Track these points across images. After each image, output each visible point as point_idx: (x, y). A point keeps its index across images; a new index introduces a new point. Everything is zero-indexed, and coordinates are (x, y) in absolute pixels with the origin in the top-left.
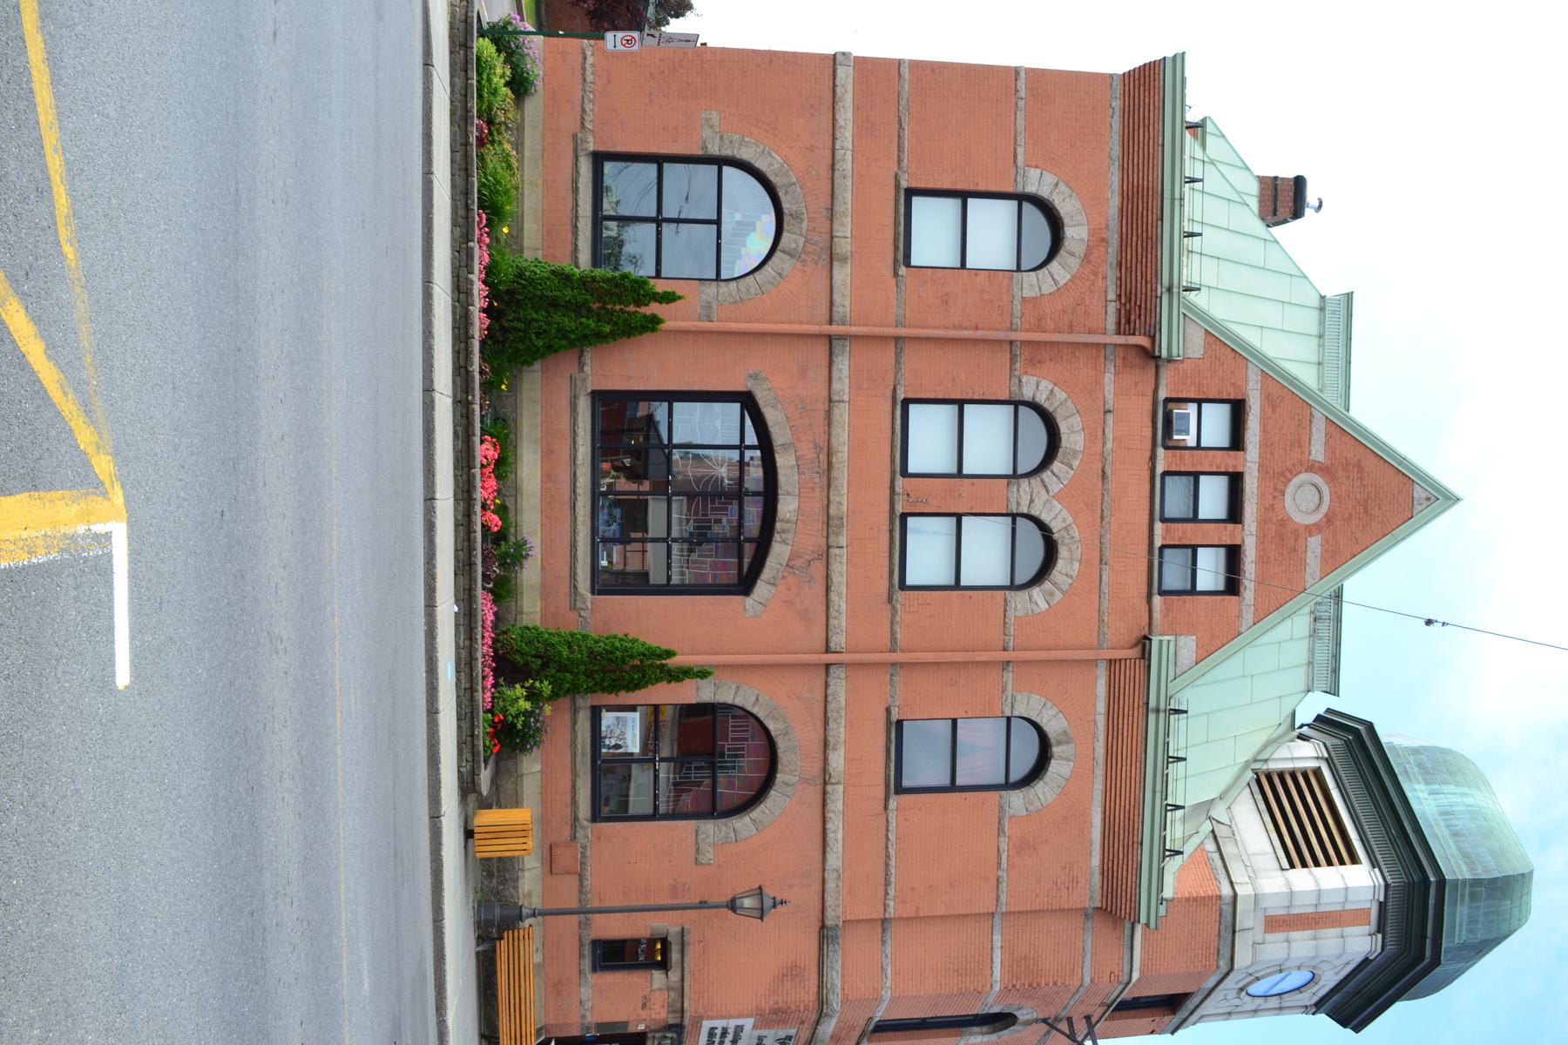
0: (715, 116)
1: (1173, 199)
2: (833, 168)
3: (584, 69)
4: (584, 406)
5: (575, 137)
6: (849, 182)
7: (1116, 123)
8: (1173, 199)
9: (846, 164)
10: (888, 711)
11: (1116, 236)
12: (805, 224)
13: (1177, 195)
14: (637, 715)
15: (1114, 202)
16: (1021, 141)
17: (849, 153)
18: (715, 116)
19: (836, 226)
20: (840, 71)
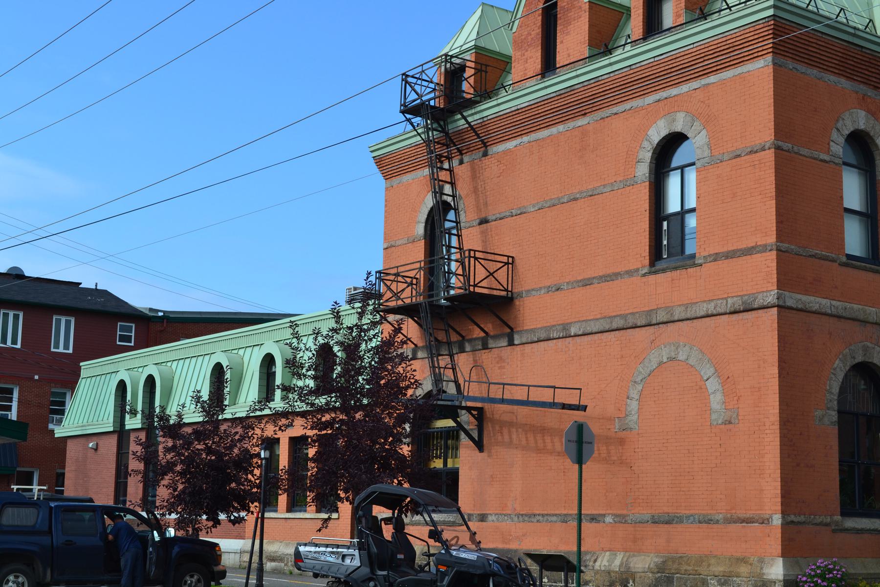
0: (818, 413)
1: (854, 35)
2: (839, 317)
3: (799, 523)
4: (851, 523)
5: (834, 531)
6: (848, 305)
7: (802, 68)
8: (854, 35)
9: (837, 306)
10: (644, 275)
11: (862, 86)
12: (869, 344)
13: (852, 31)
14: (442, 466)
15: (844, 83)
16: (816, 154)
17: (834, 303)
18: (818, 413)
19: (871, 319)
20: (790, 303)
